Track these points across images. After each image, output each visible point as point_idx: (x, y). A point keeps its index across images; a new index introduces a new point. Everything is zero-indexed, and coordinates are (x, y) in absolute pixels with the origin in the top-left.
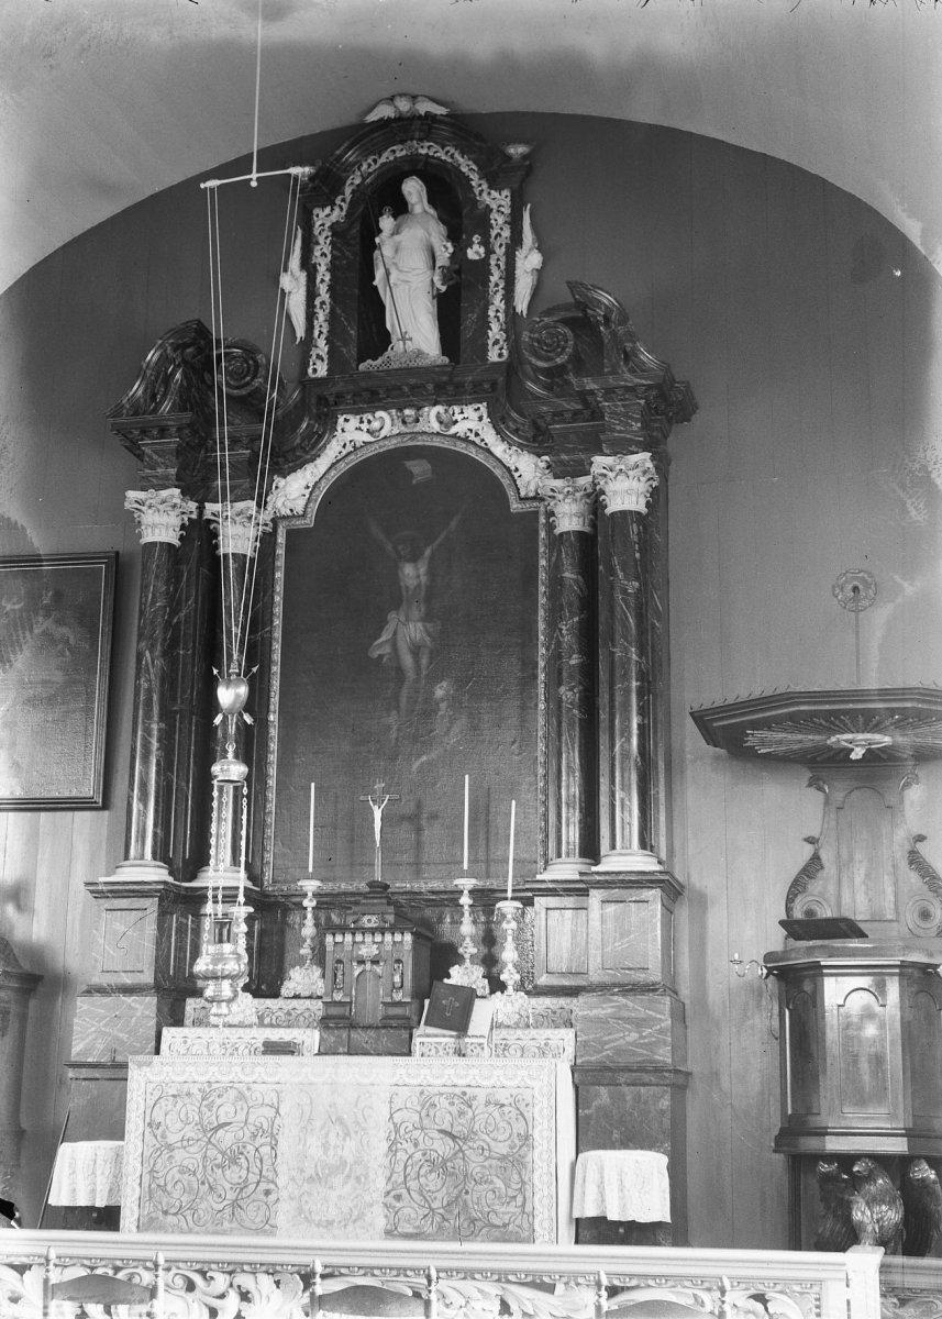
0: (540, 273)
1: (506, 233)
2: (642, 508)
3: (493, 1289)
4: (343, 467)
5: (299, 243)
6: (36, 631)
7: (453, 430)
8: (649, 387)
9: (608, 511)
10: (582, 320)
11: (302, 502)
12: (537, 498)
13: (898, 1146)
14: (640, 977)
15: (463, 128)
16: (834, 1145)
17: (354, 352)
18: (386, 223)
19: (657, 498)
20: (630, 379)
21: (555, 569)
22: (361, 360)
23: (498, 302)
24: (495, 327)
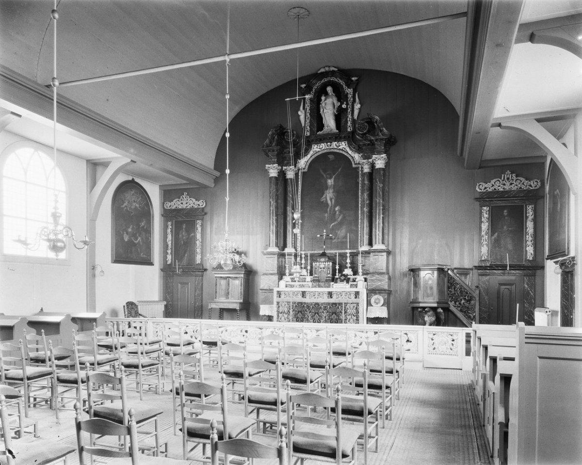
0: (360, 109)
1: (352, 99)
2: (384, 167)
3: (353, 332)
4: (313, 157)
5: (302, 103)
6: (116, 205)
7: (339, 148)
8: (386, 139)
9: (376, 168)
10: (370, 122)
11: (305, 165)
12: (359, 164)
13: (435, 305)
14: (382, 271)
15: (345, 74)
16: (421, 305)
17: (316, 129)
18: (323, 98)
19: (387, 164)
20: (381, 137)
21: (363, 180)
22: (318, 131)
23: (350, 116)
24: (349, 123)
